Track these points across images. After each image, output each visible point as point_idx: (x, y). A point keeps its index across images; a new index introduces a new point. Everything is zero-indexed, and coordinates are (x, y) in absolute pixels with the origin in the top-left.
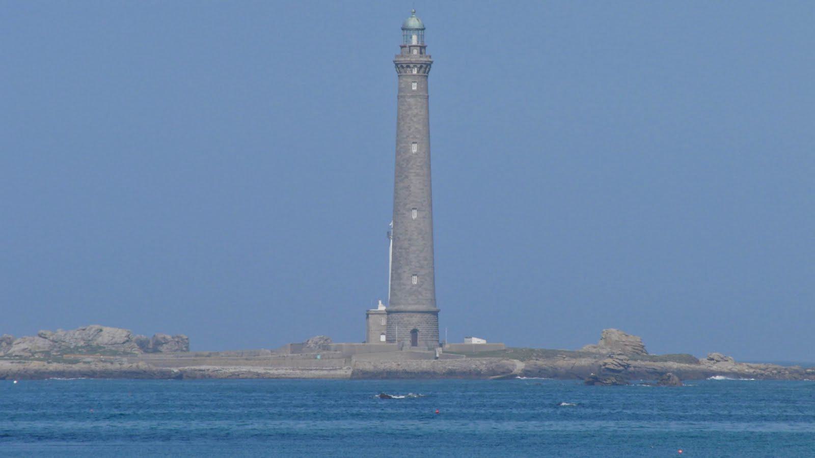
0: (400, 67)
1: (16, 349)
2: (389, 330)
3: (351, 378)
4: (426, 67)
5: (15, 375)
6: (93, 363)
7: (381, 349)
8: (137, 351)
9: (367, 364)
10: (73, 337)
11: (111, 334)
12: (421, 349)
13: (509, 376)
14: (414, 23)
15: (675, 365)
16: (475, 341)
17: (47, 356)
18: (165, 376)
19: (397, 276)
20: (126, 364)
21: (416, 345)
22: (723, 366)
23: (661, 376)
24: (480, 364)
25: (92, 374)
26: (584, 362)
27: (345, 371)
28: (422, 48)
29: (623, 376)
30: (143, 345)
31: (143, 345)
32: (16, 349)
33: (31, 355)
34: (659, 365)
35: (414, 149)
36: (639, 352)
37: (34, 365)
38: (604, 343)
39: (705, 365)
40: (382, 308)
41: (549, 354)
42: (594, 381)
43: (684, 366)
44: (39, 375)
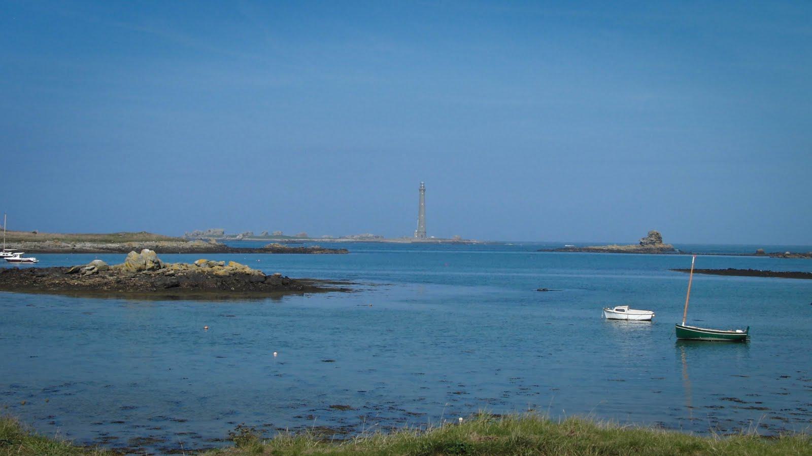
0: (420, 190)
1: (354, 237)
2: (418, 235)
3: (282, 296)
4: (424, 190)
5: (355, 242)
6: (367, 240)
7: (416, 238)
8: (375, 238)
9: (414, 241)
10: (364, 235)
11: (371, 235)
12: (423, 238)
13: (438, 243)
14: (422, 183)
15: (466, 241)
16: (432, 237)
17: (360, 238)
18: (380, 242)
19: (419, 225)
20: (373, 240)
21: (678, 343)
22: (475, 241)
23: (464, 243)
24: (433, 241)
25: (367, 242)
26: (451, 241)
27: (410, 242)
28: (424, 187)
29: (458, 243)
30: (376, 237)
31: (376, 237)
32: (354, 237)
33: (325, 238)
34: (464, 241)
35: (422, 204)
36: (460, 239)
37: (358, 240)
38: (455, 237)
39: (471, 241)
40: (416, 231)
41: (444, 239)
42: (453, 244)
43: (468, 241)
44: (358, 242)
